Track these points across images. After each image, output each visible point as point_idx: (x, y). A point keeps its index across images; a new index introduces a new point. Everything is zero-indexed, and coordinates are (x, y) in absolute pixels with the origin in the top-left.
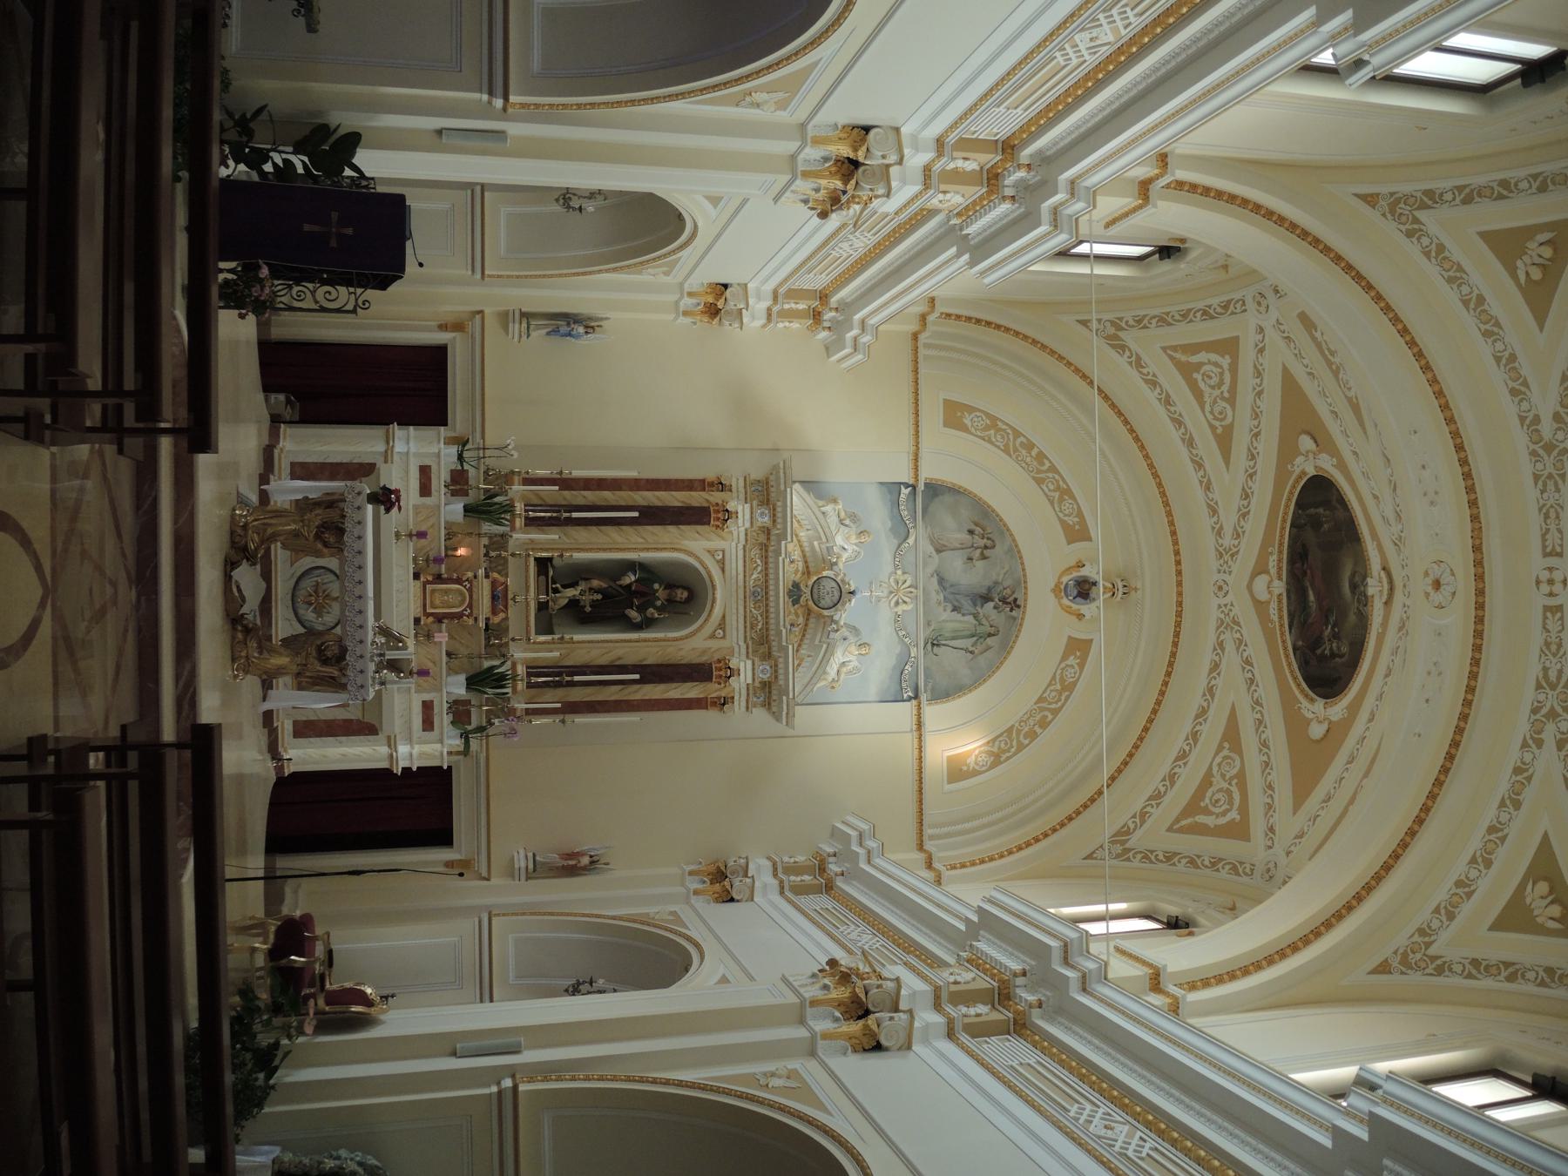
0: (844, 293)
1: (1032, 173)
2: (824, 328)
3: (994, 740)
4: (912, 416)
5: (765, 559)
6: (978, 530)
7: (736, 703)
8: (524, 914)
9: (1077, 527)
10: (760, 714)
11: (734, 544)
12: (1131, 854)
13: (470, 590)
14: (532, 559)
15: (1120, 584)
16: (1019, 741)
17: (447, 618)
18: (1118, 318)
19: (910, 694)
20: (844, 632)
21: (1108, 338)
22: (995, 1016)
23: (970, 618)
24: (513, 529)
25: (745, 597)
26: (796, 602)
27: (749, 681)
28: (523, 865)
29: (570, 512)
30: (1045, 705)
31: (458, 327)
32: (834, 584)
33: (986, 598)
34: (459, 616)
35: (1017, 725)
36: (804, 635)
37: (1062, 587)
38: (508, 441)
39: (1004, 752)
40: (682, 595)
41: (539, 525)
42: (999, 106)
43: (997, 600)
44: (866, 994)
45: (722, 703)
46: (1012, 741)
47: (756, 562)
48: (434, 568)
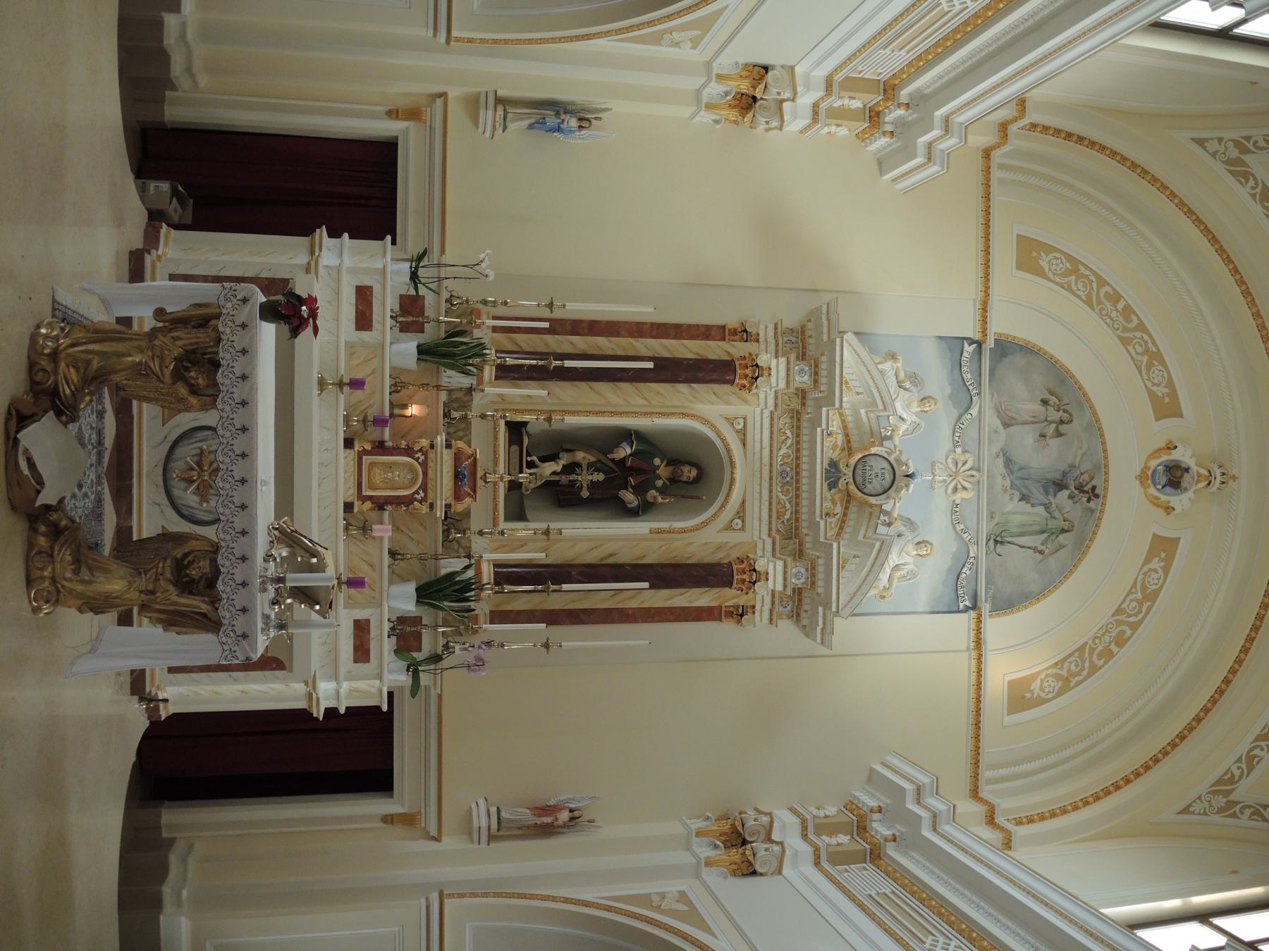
0: (922, 82)
1: (910, 111)
2: (884, 133)
3: (1063, 661)
4: (981, 254)
5: (797, 429)
6: (1053, 399)
7: (757, 613)
8: (486, 895)
9: (1167, 400)
10: (786, 627)
11: (758, 410)
12: (1237, 808)
13: (424, 465)
14: (502, 422)
15: (1218, 472)
16: (1091, 662)
17: (391, 503)
18: (1244, 138)
19: (967, 603)
20: (898, 526)
21: (1229, 162)
22: (856, 847)
23: (1040, 510)
24: (480, 381)
25: (771, 478)
26: (833, 485)
27: (779, 587)
28: (484, 823)
29: (562, 360)
30: (1122, 618)
31: (413, 114)
32: (885, 465)
33: (1060, 485)
34: (408, 501)
35: (1090, 642)
36: (841, 528)
37: (1150, 473)
38: (482, 256)
39: (1075, 675)
40: (689, 473)
41: (514, 379)
42: (885, 49)
43: (1072, 488)
44: (743, 826)
45: (739, 614)
46: (1083, 662)
47: (785, 433)
48: (374, 433)
